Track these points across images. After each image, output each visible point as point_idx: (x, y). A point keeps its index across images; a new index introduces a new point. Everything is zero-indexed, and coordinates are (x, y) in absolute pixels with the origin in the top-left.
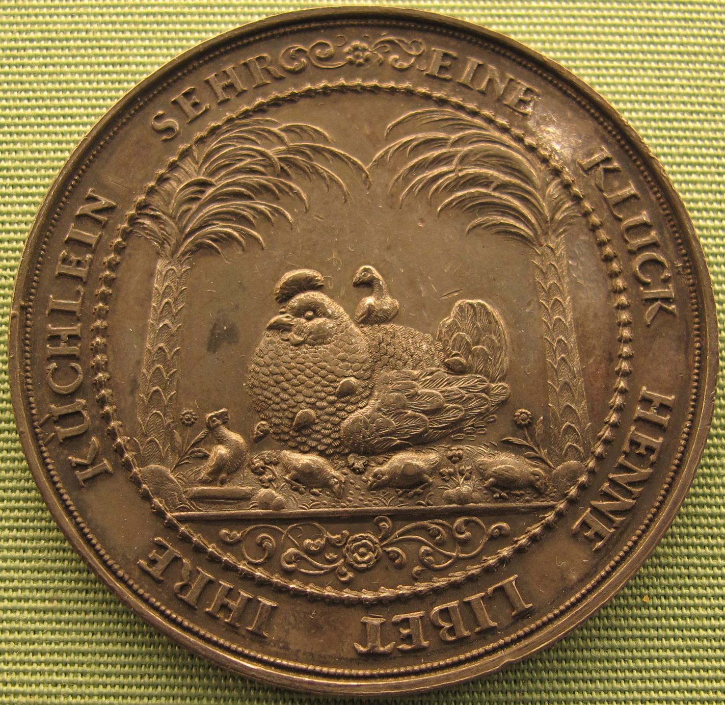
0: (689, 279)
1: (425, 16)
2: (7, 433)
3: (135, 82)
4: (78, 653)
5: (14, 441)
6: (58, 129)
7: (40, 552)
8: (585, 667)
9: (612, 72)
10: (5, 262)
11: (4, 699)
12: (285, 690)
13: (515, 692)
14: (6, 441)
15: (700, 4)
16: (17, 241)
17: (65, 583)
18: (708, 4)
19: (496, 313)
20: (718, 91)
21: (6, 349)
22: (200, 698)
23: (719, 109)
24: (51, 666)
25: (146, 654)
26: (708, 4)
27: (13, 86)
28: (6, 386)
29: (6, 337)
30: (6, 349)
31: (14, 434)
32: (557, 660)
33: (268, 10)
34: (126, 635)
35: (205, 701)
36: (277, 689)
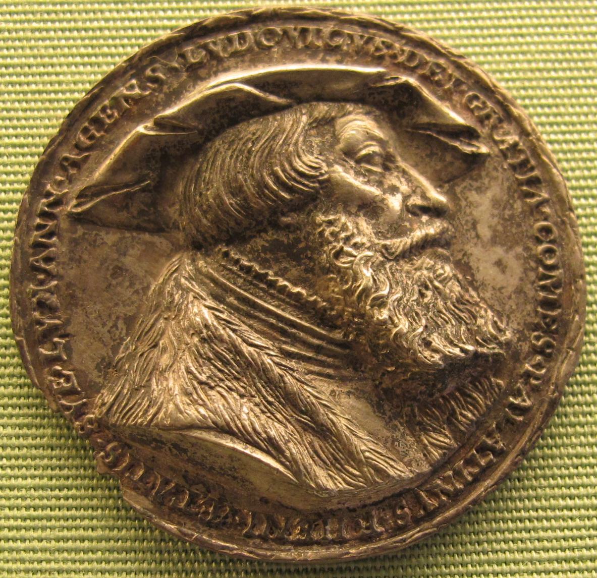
0: (132, 87)
2: (6, 530)
4: (68, 540)
5: (13, 356)
7: (35, 469)
8: (472, 530)
10: (6, 554)
15: (397, 5)
17: (54, 460)
18: (405, 4)
19: (125, 104)
20: (590, 182)
21: (8, 312)
23: (591, 73)
24: (38, 461)
26: (405, 4)
27: (86, 59)
28: (5, 311)
29: (6, 271)
30: (7, 282)
32: (470, 543)
33: (201, 13)
35: (158, 576)
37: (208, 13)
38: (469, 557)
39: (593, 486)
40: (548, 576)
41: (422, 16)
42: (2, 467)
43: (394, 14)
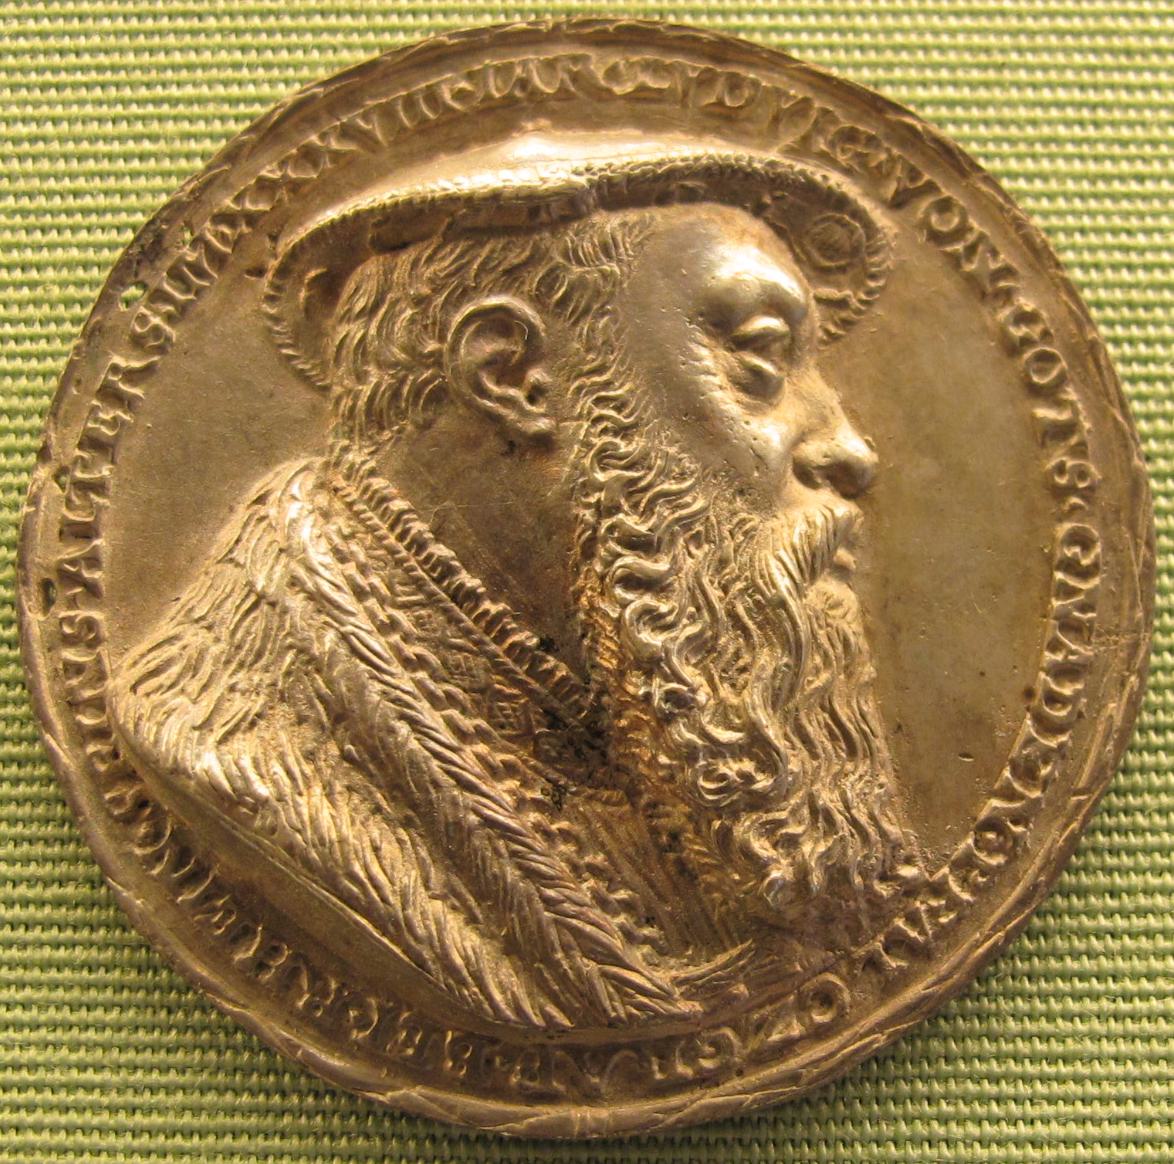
1: (653, 135)
3: (168, 192)
6: (67, 42)
9: (1108, 132)
11: (1163, 7)
12: (418, 1116)
13: (896, 1119)
14: (13, 821)
16: (34, 394)
22: (280, 1155)
25: (195, 1047)
31: (18, 690)
34: (170, 1012)
36: (403, 1115)
37: (387, 38)
38: (1119, 942)
39: (1165, 1080)
40: (111, 1160)
41: (820, 38)
42: (4, 18)
43: (857, 66)
